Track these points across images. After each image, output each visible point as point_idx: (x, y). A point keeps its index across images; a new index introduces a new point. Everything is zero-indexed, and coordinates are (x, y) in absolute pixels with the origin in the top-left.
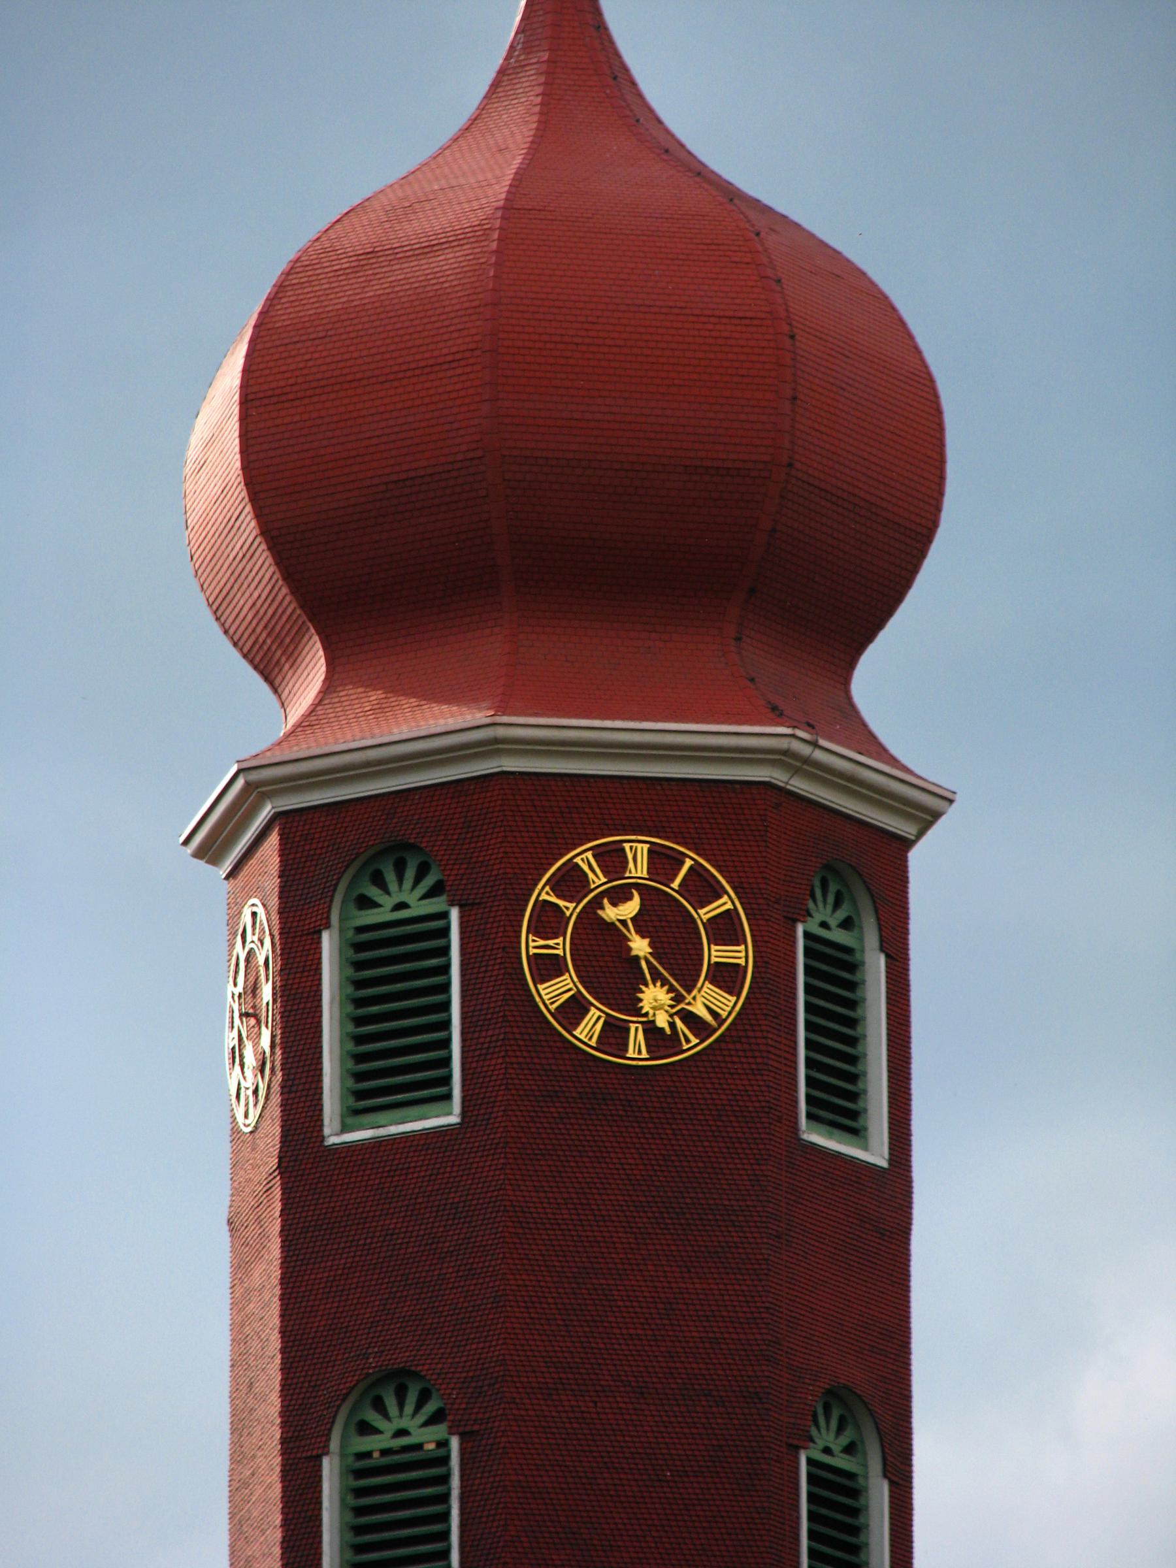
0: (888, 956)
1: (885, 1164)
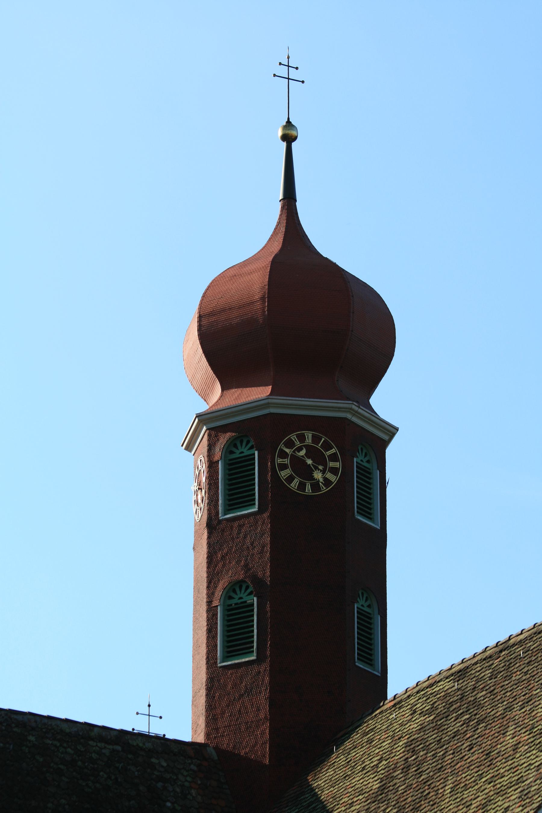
0: (381, 616)
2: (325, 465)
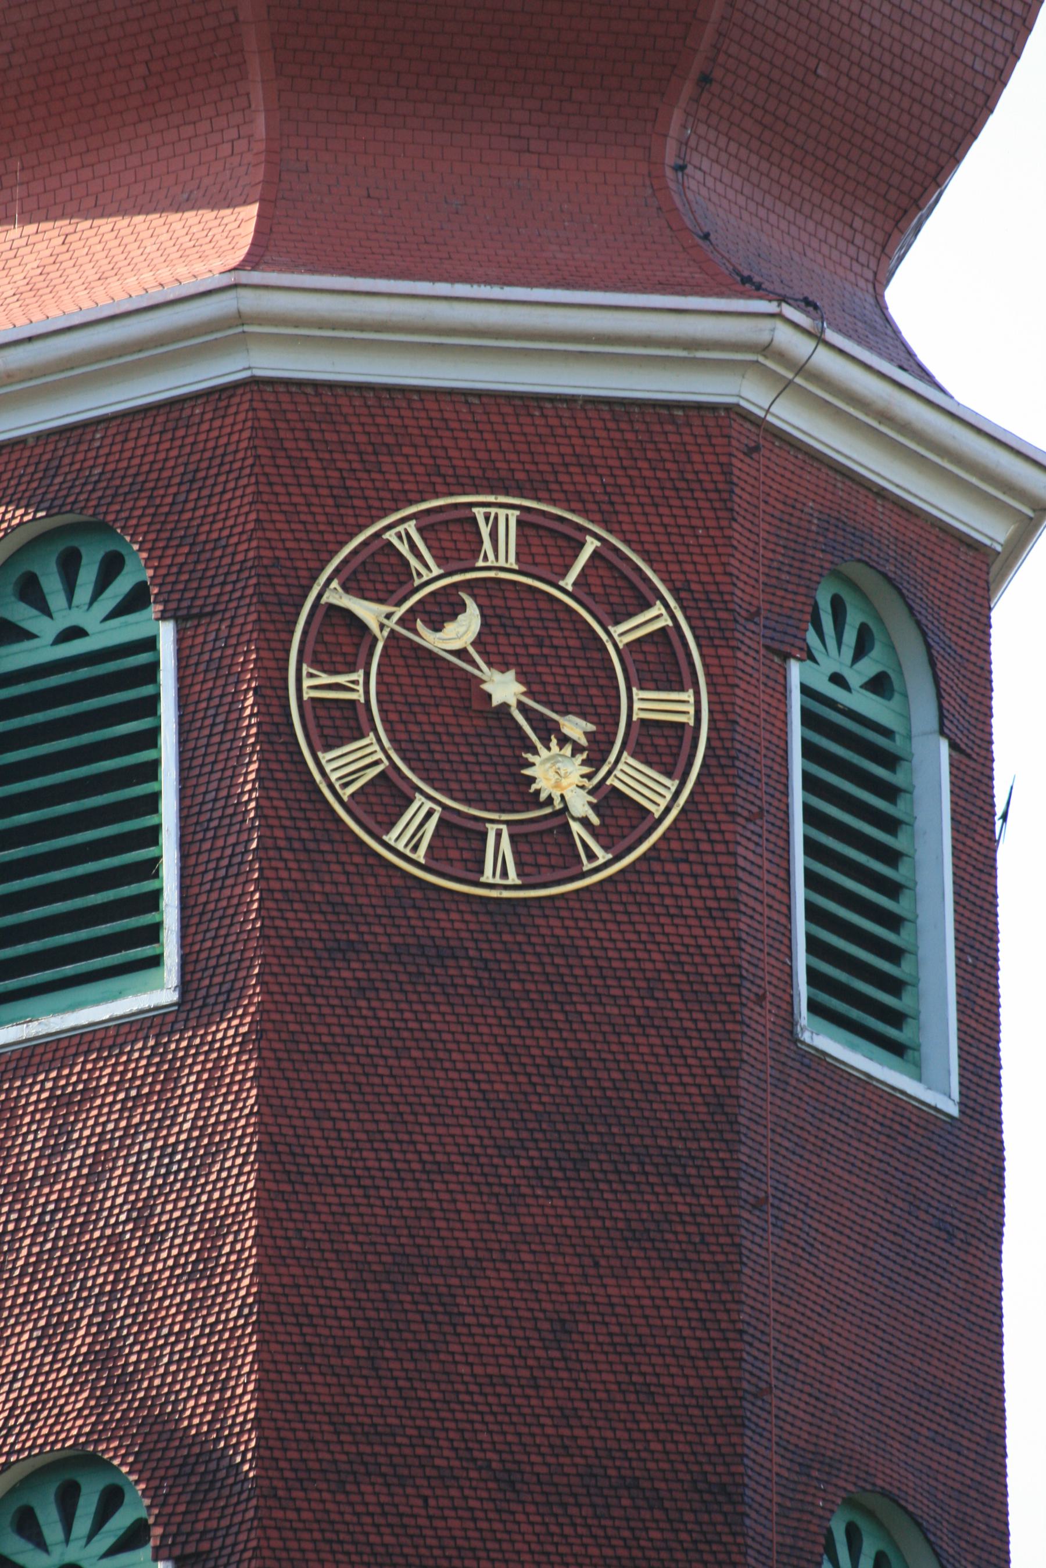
0: (953, 746)
1: (954, 1111)
2: (603, 712)
